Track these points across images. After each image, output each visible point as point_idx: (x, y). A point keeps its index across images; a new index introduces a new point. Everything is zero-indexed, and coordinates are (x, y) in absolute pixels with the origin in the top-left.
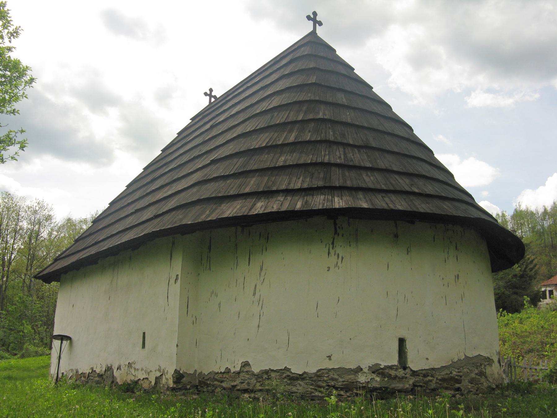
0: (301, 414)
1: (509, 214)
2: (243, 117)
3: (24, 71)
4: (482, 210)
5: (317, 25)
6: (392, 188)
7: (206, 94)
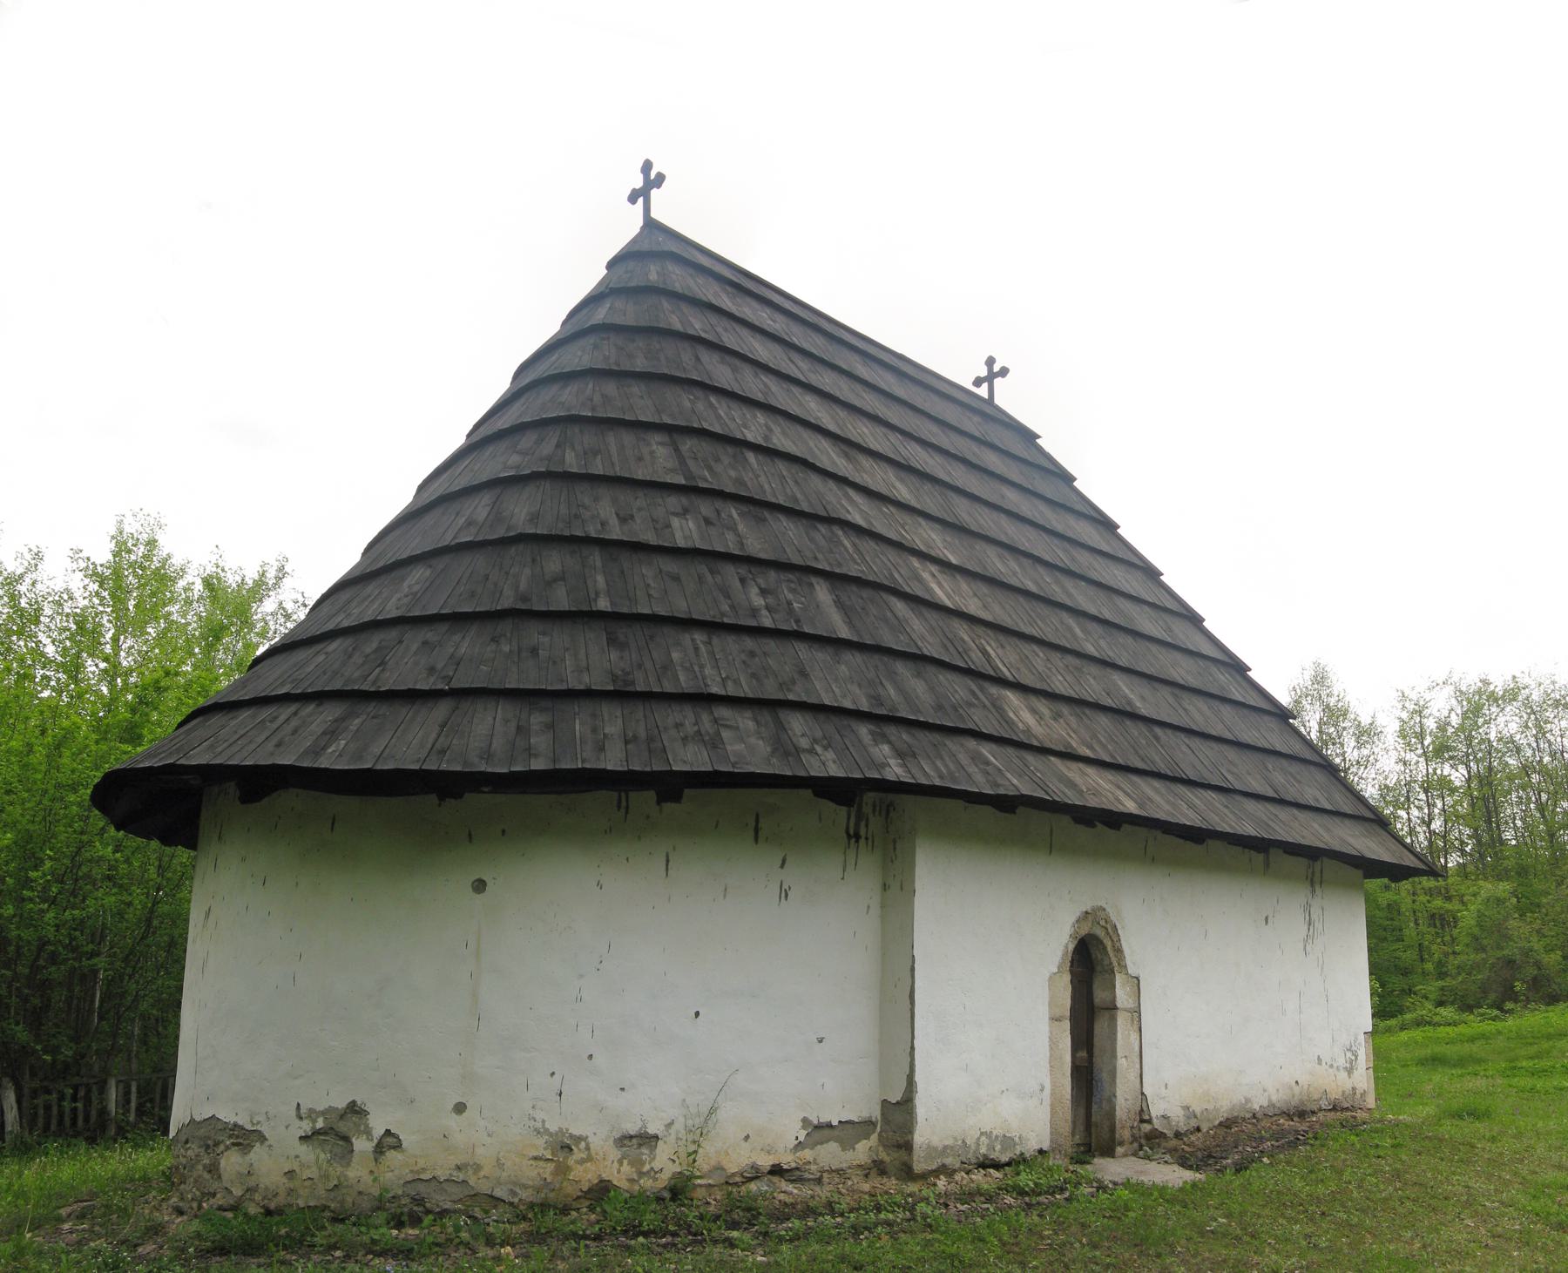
7: (990, 362)
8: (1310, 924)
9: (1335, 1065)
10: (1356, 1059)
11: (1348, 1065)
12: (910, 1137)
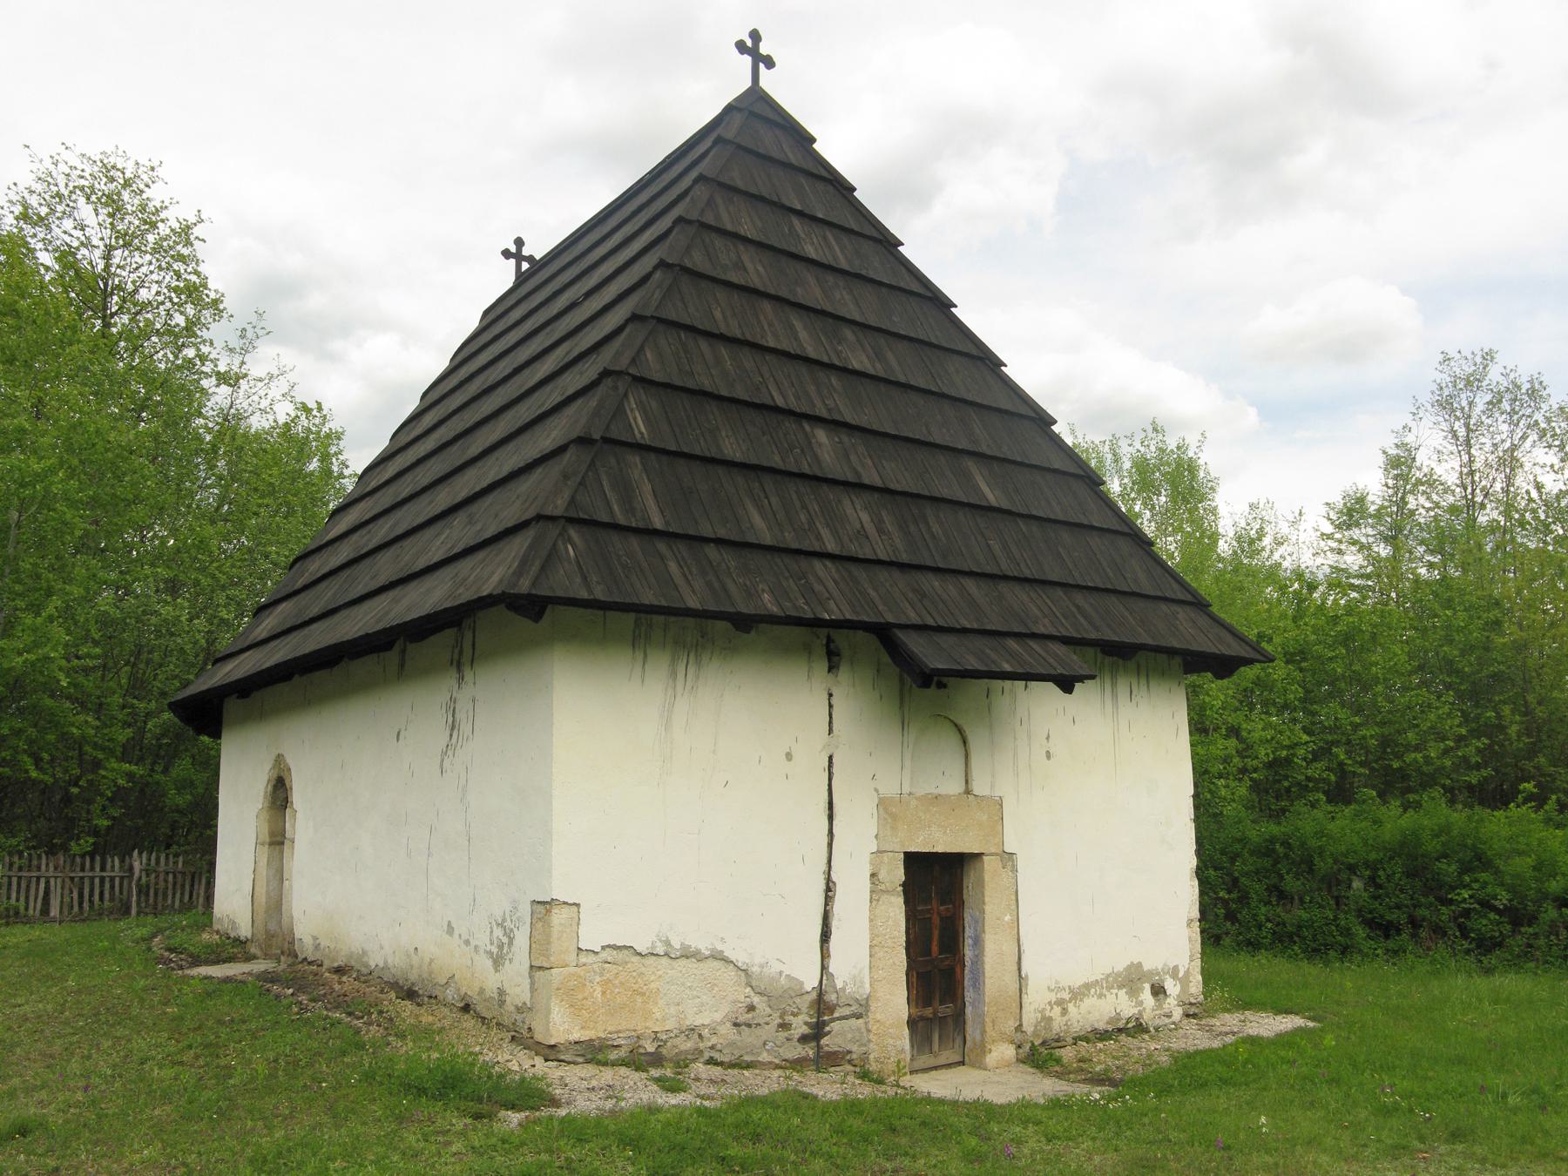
0: (259, 1174)
1: (219, 916)
2: (702, 1097)
3: (430, 975)
4: (839, 182)
5: (762, 66)
6: (1109, 586)
7: (506, 254)
8: (453, 729)
9: (473, 943)
10: (511, 943)
11: (495, 950)
12: (216, 980)
